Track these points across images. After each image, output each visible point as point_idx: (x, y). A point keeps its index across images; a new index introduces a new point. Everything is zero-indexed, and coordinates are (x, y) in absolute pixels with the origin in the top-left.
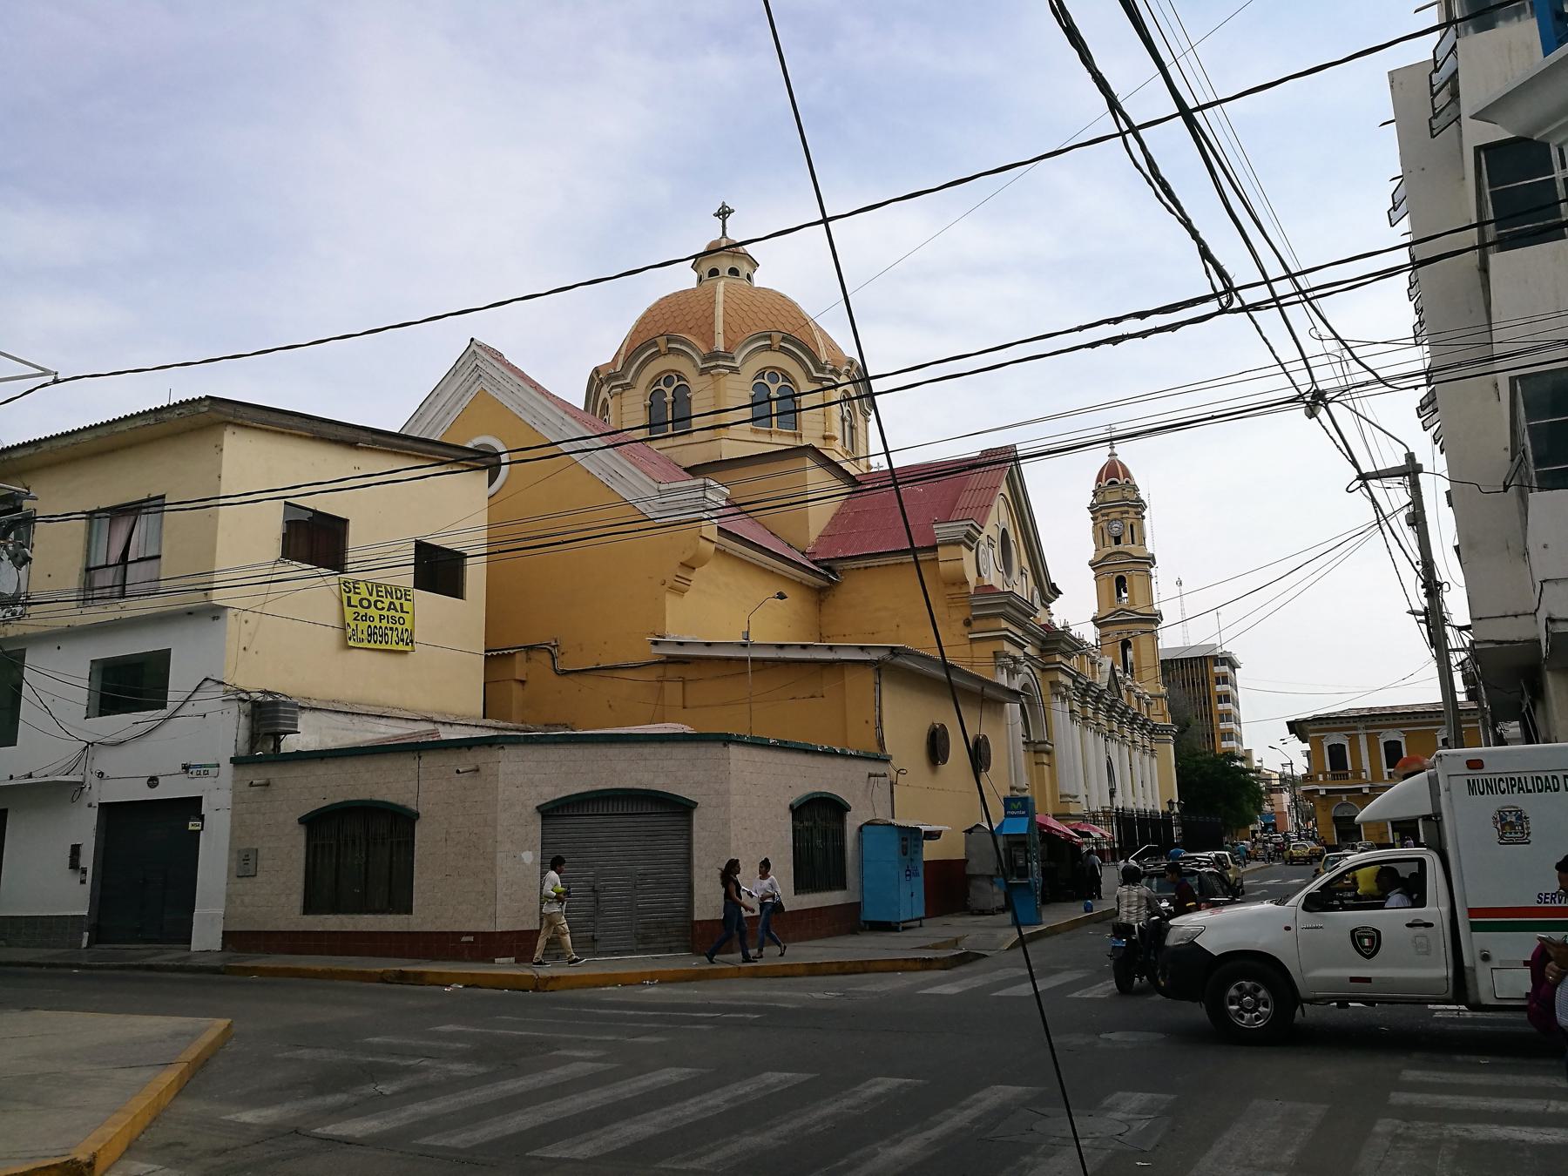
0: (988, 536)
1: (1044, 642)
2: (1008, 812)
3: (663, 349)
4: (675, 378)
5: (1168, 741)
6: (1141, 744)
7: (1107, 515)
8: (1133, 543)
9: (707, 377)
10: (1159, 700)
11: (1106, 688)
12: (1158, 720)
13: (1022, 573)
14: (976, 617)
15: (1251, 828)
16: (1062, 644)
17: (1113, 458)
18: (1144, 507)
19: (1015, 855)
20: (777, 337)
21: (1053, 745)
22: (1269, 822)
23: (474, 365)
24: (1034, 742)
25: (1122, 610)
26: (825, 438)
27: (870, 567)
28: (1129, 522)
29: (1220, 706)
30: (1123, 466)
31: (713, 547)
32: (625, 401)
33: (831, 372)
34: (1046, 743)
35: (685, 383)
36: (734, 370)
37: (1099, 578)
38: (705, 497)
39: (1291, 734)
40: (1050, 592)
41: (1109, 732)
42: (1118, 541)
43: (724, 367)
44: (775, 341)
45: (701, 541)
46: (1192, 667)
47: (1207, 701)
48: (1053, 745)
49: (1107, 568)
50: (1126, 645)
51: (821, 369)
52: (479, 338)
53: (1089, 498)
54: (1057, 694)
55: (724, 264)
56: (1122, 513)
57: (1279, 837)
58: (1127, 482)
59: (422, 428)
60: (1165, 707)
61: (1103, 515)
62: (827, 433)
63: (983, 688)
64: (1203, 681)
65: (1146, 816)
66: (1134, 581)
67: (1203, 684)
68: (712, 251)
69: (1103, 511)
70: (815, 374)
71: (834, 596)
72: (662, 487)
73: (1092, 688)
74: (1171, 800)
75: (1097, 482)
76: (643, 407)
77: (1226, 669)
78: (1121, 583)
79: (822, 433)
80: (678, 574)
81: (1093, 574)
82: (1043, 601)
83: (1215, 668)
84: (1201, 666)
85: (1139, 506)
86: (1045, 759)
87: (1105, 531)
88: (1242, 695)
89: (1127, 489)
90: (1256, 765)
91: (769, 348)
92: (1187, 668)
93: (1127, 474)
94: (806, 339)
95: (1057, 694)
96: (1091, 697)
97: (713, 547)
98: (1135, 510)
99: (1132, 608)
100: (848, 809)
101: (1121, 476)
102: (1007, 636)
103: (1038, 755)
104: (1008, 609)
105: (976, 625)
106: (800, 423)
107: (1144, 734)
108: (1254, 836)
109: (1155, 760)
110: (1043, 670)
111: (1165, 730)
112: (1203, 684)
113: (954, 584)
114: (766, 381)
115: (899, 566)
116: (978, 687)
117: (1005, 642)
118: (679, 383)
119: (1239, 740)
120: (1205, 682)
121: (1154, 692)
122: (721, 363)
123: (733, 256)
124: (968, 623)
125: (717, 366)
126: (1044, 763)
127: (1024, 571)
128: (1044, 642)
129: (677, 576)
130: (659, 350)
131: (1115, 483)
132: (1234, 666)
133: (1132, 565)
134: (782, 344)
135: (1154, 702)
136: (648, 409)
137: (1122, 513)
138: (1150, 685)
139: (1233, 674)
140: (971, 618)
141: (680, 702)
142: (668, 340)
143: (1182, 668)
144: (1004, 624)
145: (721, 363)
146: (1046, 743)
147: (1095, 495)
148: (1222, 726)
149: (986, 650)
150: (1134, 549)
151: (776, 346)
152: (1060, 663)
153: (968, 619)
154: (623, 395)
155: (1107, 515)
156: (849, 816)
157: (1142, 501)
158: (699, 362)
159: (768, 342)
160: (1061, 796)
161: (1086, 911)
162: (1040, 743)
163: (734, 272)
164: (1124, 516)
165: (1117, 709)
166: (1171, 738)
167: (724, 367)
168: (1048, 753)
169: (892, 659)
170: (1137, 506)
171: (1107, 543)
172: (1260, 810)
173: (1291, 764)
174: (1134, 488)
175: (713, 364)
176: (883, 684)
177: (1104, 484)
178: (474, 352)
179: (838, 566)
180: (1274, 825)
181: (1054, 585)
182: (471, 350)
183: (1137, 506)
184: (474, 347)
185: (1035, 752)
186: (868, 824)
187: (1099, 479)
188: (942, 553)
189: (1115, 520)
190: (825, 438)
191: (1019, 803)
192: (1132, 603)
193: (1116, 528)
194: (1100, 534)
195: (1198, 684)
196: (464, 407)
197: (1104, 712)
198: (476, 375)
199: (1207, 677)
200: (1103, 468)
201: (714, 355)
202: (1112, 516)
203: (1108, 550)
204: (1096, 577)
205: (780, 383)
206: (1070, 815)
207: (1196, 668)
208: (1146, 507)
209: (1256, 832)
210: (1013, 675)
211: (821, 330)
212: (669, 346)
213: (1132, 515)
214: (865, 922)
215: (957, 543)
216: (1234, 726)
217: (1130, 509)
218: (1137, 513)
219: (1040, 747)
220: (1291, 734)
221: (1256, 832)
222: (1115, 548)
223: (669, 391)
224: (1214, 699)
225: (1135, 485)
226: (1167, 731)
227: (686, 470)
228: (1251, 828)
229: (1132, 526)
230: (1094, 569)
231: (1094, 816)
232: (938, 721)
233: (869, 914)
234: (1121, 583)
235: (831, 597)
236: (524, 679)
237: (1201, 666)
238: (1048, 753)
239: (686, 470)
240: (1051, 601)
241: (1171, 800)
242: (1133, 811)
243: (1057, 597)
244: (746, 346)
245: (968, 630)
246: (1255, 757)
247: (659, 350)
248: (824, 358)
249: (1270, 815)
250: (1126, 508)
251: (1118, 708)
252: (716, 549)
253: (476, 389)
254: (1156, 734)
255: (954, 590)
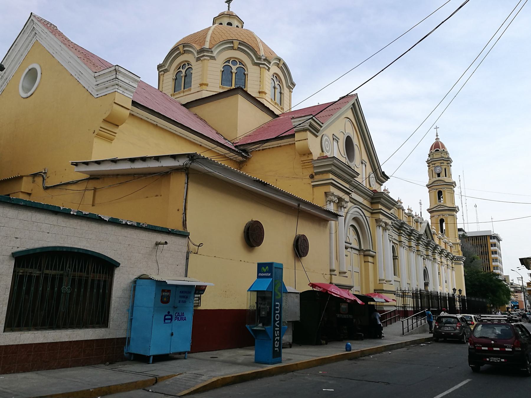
0: (333, 135)
1: (372, 198)
2: (260, 274)
3: (182, 51)
4: (187, 64)
5: (461, 264)
6: (451, 266)
7: (434, 164)
8: (446, 176)
9: (200, 62)
10: (456, 245)
11: (423, 234)
12: (457, 255)
13: (362, 163)
14: (317, 173)
15: (507, 306)
16: (382, 199)
17: (437, 140)
18: (451, 162)
19: (260, 307)
20: (236, 44)
21: (376, 253)
22: (516, 304)
23: (32, 27)
24: (363, 250)
25: (440, 205)
26: (260, 92)
27: (265, 149)
28: (444, 167)
29: (493, 256)
30: (441, 143)
31: (128, 112)
32: (165, 78)
33: (265, 60)
34: (370, 250)
35: (191, 66)
36: (213, 58)
37: (431, 192)
38: (116, 78)
39: (522, 265)
40: (381, 176)
41: (433, 259)
42: (439, 175)
43: (207, 56)
44: (235, 45)
45: (115, 105)
46: (480, 239)
47: (487, 253)
48: (376, 253)
49: (433, 187)
50: (442, 221)
51: (259, 59)
52: (35, 13)
53: (427, 158)
54: (379, 226)
55: (225, 21)
56: (441, 163)
57: (519, 311)
58: (443, 150)
59: (9, 63)
60: (460, 249)
61: (432, 164)
62: (260, 90)
63: (299, 205)
64: (485, 244)
65: (438, 294)
66: (446, 194)
67: (485, 247)
68: (222, 15)
69: (433, 163)
70: (256, 61)
71: (246, 165)
72: (96, 75)
73: (414, 232)
74: (460, 289)
75: (430, 150)
76: (172, 80)
77: (495, 241)
78: (440, 193)
79: (258, 90)
80: (102, 126)
81: (428, 190)
82: (378, 181)
83: (491, 240)
84: (485, 239)
85: (449, 161)
86: (370, 259)
87: (434, 171)
88: (502, 252)
89: (443, 153)
90: (510, 282)
91: (232, 48)
92: (478, 240)
93: (443, 146)
94: (253, 46)
95: (379, 226)
96: (414, 237)
97: (128, 112)
98: (447, 162)
99: (445, 205)
100: (116, 265)
101: (441, 148)
102: (332, 183)
103: (365, 257)
104: (333, 167)
105: (317, 177)
106: (247, 85)
107: (448, 259)
108: (508, 311)
109: (454, 272)
110: (372, 213)
111: (459, 259)
112: (485, 247)
113: (304, 155)
114: (230, 64)
115: (279, 148)
116: (295, 204)
117: (331, 187)
118: (189, 67)
119: (502, 270)
120: (486, 246)
121: (454, 242)
122: (205, 54)
123: (230, 17)
124: (312, 177)
125: (204, 56)
126: (368, 262)
127: (363, 162)
128: (372, 198)
129: (101, 127)
130: (180, 52)
131: (438, 150)
132: (499, 240)
133: (445, 186)
134: (239, 46)
135: (454, 246)
136: (174, 80)
137: (441, 163)
138: (453, 238)
139: (498, 243)
140: (314, 174)
141: (91, 203)
142: (183, 46)
143: (476, 240)
144: (331, 176)
145: (205, 54)
146: (370, 250)
147: (429, 156)
148: (494, 264)
149: (320, 192)
150: (447, 179)
151: (236, 47)
152: (381, 209)
153: (312, 174)
154: (164, 75)
155: (434, 164)
156: (117, 273)
157: (450, 158)
158: (196, 54)
159: (232, 45)
160: (380, 280)
161: (347, 351)
162: (366, 251)
163: (230, 24)
164: (442, 164)
165: (430, 245)
166: (463, 263)
167: (207, 56)
168: (373, 257)
169: (191, 164)
170: (448, 161)
171: (434, 176)
172: (509, 299)
173: (522, 278)
174: (446, 153)
175: (202, 55)
176: (189, 184)
177: (433, 151)
178: (32, 20)
179: (249, 148)
180: (518, 306)
181: (383, 173)
182: (31, 19)
183: (448, 161)
184: (32, 17)
185: (365, 255)
186: (140, 278)
187: (431, 149)
188: (298, 136)
189: (438, 166)
190: (260, 92)
191: (267, 267)
192: (445, 202)
193: (438, 170)
194: (431, 173)
195: (483, 247)
196: (28, 51)
197: (438, 254)
198: (33, 33)
199: (487, 244)
200: (434, 143)
201: (202, 50)
202: (436, 165)
203: (435, 179)
204: (429, 191)
205: (238, 66)
206: (383, 290)
207: (482, 240)
208: (452, 161)
209: (509, 308)
210: (386, 230)
211: (263, 44)
212: (184, 49)
213: (445, 164)
214: (131, 354)
215: (305, 130)
216: (499, 264)
217: (444, 162)
218: (448, 164)
219: (367, 253)
220: (522, 265)
221: (509, 308)
222: (438, 178)
223: (184, 71)
224: (490, 253)
225: (447, 151)
226: (460, 259)
227: (184, 105)
228: (507, 306)
229: (445, 169)
230: (428, 188)
231: (403, 293)
232: (300, 232)
233: (134, 348)
234: (440, 193)
235: (245, 166)
236: (30, 193)
237: (485, 239)
238: (373, 257)
239: (184, 105)
240: (384, 182)
241: (460, 289)
242: (437, 293)
243: (387, 180)
244: (219, 46)
245: (312, 180)
246: (511, 279)
247: (180, 52)
248: (262, 53)
249: (516, 302)
250: (443, 161)
251: (431, 245)
252: (130, 114)
253: (34, 40)
254: (454, 260)
255: (305, 158)
